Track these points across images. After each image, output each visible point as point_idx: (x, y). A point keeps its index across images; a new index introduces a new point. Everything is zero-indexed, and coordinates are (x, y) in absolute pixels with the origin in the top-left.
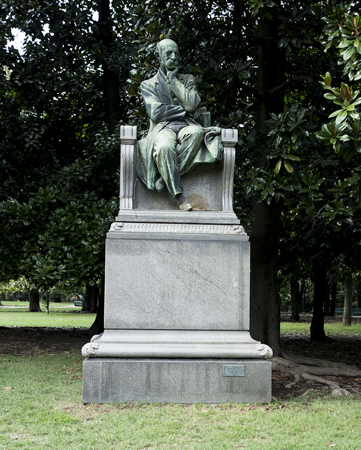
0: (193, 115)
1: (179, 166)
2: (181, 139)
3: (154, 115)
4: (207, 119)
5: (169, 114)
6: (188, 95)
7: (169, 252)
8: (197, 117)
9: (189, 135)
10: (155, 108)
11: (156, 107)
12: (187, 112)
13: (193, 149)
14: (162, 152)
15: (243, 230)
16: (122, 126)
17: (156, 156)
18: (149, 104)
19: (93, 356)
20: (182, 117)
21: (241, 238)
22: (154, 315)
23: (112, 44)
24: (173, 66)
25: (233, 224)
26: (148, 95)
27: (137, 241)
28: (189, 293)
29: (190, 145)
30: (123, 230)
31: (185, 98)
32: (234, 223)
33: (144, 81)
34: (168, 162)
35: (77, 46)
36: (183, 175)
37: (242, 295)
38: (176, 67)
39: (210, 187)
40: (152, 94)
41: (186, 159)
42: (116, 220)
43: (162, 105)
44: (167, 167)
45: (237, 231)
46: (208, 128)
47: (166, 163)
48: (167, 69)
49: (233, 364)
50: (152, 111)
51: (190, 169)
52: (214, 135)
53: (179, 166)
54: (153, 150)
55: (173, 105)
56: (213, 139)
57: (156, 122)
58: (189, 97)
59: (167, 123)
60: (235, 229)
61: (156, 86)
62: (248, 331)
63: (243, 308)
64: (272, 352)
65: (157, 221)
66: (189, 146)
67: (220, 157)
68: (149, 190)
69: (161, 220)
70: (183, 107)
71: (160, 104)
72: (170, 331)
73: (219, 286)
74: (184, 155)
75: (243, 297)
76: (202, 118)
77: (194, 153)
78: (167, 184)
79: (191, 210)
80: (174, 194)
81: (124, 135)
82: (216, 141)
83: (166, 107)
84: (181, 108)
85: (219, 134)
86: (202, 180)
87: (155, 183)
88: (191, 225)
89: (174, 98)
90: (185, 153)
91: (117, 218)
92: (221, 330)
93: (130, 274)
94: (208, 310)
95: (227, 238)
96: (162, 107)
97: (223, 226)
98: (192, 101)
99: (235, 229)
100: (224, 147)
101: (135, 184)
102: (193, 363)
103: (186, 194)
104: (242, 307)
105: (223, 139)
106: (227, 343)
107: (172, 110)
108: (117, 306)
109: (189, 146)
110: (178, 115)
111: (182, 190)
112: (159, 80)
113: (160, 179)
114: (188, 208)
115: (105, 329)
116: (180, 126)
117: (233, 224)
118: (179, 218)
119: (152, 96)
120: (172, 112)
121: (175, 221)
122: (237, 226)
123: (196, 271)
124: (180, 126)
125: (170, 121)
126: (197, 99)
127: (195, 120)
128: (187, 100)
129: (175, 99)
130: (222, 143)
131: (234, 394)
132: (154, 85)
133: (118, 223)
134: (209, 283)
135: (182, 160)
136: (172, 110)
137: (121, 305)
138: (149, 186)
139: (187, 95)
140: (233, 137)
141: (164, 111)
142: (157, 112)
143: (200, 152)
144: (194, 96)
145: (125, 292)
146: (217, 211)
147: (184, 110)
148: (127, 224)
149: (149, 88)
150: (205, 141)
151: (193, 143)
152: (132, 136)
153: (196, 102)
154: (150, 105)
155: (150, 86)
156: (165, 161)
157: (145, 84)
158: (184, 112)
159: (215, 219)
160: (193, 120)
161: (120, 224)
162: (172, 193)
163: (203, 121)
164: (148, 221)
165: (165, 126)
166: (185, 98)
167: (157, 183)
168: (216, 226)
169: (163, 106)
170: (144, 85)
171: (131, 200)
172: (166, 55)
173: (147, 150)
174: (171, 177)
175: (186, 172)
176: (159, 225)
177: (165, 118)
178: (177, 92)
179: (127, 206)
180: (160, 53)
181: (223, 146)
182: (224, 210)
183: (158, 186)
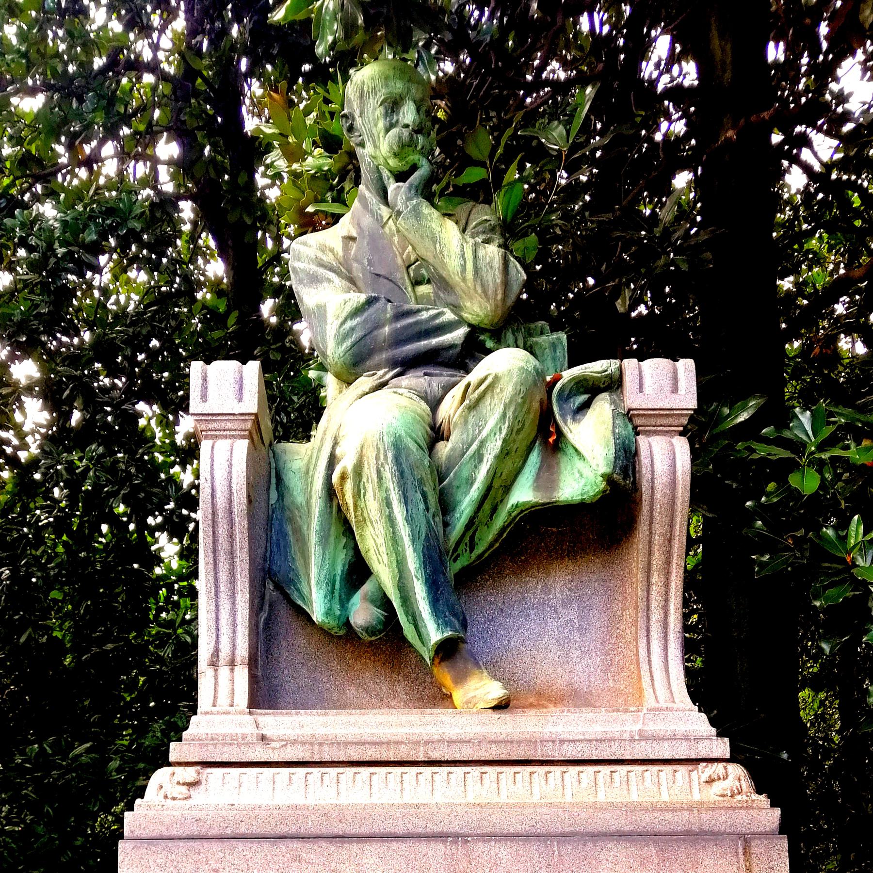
3: (339, 343)
4: (554, 359)
5: (399, 340)
6: (475, 257)
9: (486, 378)
10: (341, 320)
11: (348, 309)
13: (505, 441)
15: (746, 784)
17: (343, 478)
20: (452, 346)
21: (742, 821)
26: (314, 280)
27: (266, 845)
30: (198, 796)
31: (464, 268)
36: (463, 570)
39: (581, 618)
40: (332, 275)
41: (475, 492)
43: (370, 302)
44: (391, 520)
45: (719, 787)
47: (388, 504)
48: (386, 173)
51: (495, 540)
56: (586, 406)
57: (347, 379)
58: (481, 263)
59: (391, 374)
60: (710, 781)
61: (346, 249)
65: (355, 758)
66: (484, 433)
68: (320, 629)
70: (456, 308)
71: (362, 298)
77: (509, 465)
78: (396, 603)
79: (502, 706)
81: (204, 397)
83: (385, 311)
87: (344, 602)
95: (680, 821)
96: (371, 310)
97: (654, 769)
98: (490, 279)
101: (264, 616)
103: (475, 642)
107: (411, 320)
109: (484, 433)
110: (434, 341)
111: (464, 625)
112: (359, 226)
113: (368, 587)
118: (451, 742)
119: (329, 281)
120: (410, 331)
121: (435, 755)
122: (719, 768)
125: (406, 365)
126: (512, 272)
128: (470, 274)
130: (629, 416)
136: (411, 320)
138: (318, 613)
139: (469, 255)
140: (675, 390)
141: (378, 326)
142: (352, 329)
143: (534, 458)
147: (461, 322)
149: (320, 255)
151: (504, 415)
152: (240, 400)
156: (381, 495)
161: (190, 773)
164: (316, 758)
166: (464, 268)
168: (622, 769)
172: (379, 111)
173: (307, 472)
174: (413, 562)
176: (365, 771)
177: (384, 356)
178: (428, 243)
180: (357, 114)
181: (635, 428)
182: (649, 701)
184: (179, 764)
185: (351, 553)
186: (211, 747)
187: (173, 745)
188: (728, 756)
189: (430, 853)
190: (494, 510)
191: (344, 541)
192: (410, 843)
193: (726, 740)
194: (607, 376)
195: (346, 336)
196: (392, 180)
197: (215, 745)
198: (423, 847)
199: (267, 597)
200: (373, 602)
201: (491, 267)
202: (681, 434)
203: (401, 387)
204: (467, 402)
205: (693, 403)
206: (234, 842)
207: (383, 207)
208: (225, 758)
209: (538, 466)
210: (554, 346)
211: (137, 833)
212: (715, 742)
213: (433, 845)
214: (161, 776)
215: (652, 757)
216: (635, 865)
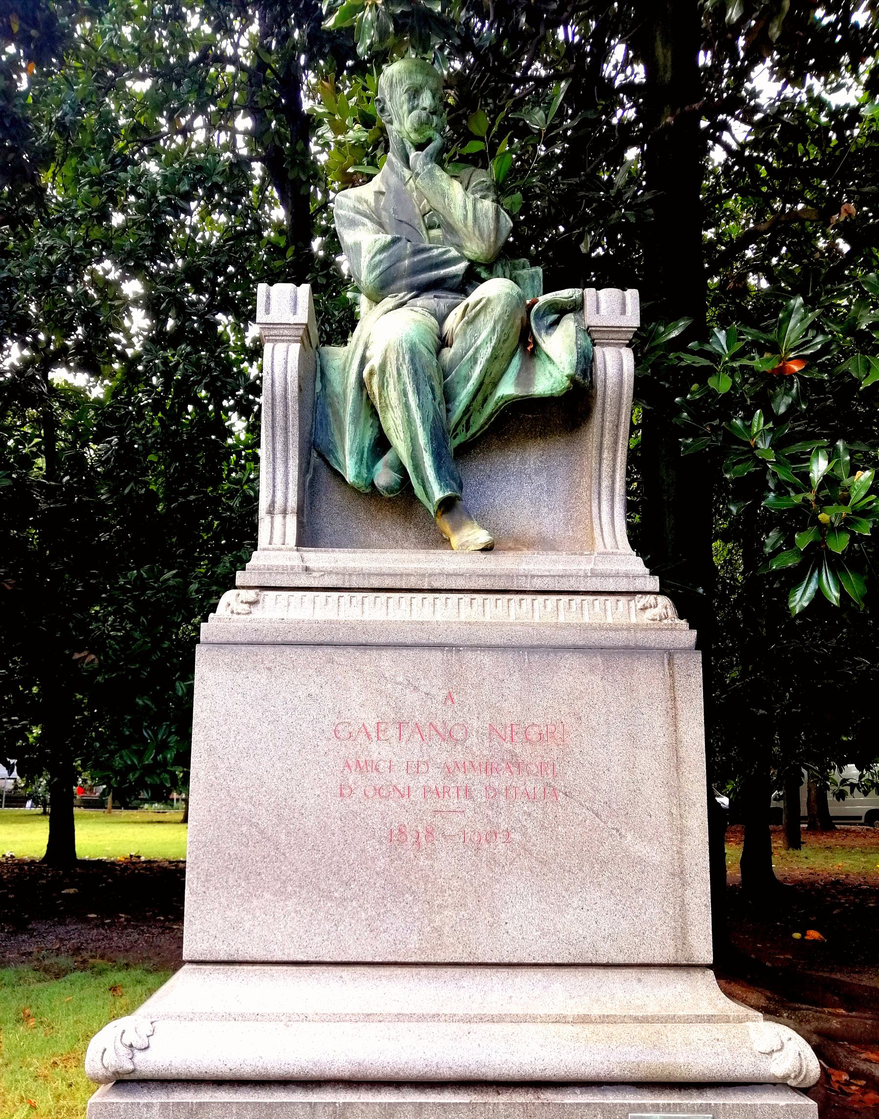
3: (371, 272)
4: (532, 287)
5: (416, 270)
7: (416, 689)
9: (480, 301)
10: (372, 254)
11: (378, 246)
12: (473, 264)
13: (494, 348)
14: (392, 357)
15: (671, 611)
16: (262, 288)
19: (126, 1077)
20: (455, 276)
21: (667, 639)
22: (366, 910)
25: (635, 593)
26: (353, 224)
29: (484, 334)
30: (257, 613)
31: (466, 217)
32: (639, 589)
34: (410, 389)
37: (682, 832)
39: (549, 483)
40: (366, 221)
41: (470, 387)
42: (238, 583)
43: (394, 241)
44: (407, 406)
45: (650, 613)
47: (405, 395)
48: (408, 144)
52: (561, 311)
54: (363, 361)
55: (427, 244)
56: (556, 323)
59: (409, 296)
60: (644, 609)
62: (709, 967)
66: (479, 342)
67: (584, 373)
68: (353, 489)
69: (388, 583)
70: (459, 247)
71: (389, 238)
72: (423, 971)
75: (682, 841)
77: (497, 367)
78: (410, 470)
79: (487, 549)
81: (267, 311)
82: (568, 324)
84: (454, 253)
85: (577, 307)
86: (523, 462)
87: (370, 467)
88: (492, 597)
90: (467, 367)
93: (278, 765)
98: (485, 225)
99: (644, 609)
101: (309, 477)
102: (513, 1105)
104: (680, 875)
106: (637, 1020)
107: (425, 256)
108: (231, 882)
109: (479, 342)
110: (442, 272)
111: (461, 487)
112: (387, 183)
113: (388, 457)
114: (479, 541)
115: (184, 962)
116: (449, 301)
117: (635, 593)
118: (449, 575)
119: (364, 225)
120: (425, 264)
121: (437, 585)
122: (651, 599)
124: (449, 301)
126: (503, 221)
130: (588, 331)
133: (242, 592)
135: (458, 390)
136: (425, 256)
137: (247, 878)
138: (350, 472)
139: (470, 207)
140: (623, 312)
141: (400, 259)
142: (381, 261)
143: (516, 362)
145: (262, 832)
148: (272, 594)
149: (357, 205)
150: (533, 325)
151: (494, 329)
152: (295, 313)
153: (497, 229)
155: (360, 200)
158: (462, 266)
159: (571, 576)
161: (251, 595)
164: (347, 585)
166: (466, 217)
167: (380, 466)
168: (577, 598)
169: (400, 244)
171: (292, 522)
173: (344, 369)
174: (423, 439)
175: (473, 431)
176: (383, 596)
178: (439, 198)
179: (277, 539)
182: (600, 548)
183: (383, 476)
185: (376, 430)
188: (658, 590)
191: (371, 421)
192: (417, 650)
193: (657, 577)
194: (572, 301)
195: (375, 267)
196: (413, 149)
198: (426, 654)
199: (312, 463)
200: (392, 468)
201: (486, 217)
202: (628, 346)
205: (636, 322)
210: (532, 277)
211: (210, 639)
212: (648, 579)
216: (586, 671)
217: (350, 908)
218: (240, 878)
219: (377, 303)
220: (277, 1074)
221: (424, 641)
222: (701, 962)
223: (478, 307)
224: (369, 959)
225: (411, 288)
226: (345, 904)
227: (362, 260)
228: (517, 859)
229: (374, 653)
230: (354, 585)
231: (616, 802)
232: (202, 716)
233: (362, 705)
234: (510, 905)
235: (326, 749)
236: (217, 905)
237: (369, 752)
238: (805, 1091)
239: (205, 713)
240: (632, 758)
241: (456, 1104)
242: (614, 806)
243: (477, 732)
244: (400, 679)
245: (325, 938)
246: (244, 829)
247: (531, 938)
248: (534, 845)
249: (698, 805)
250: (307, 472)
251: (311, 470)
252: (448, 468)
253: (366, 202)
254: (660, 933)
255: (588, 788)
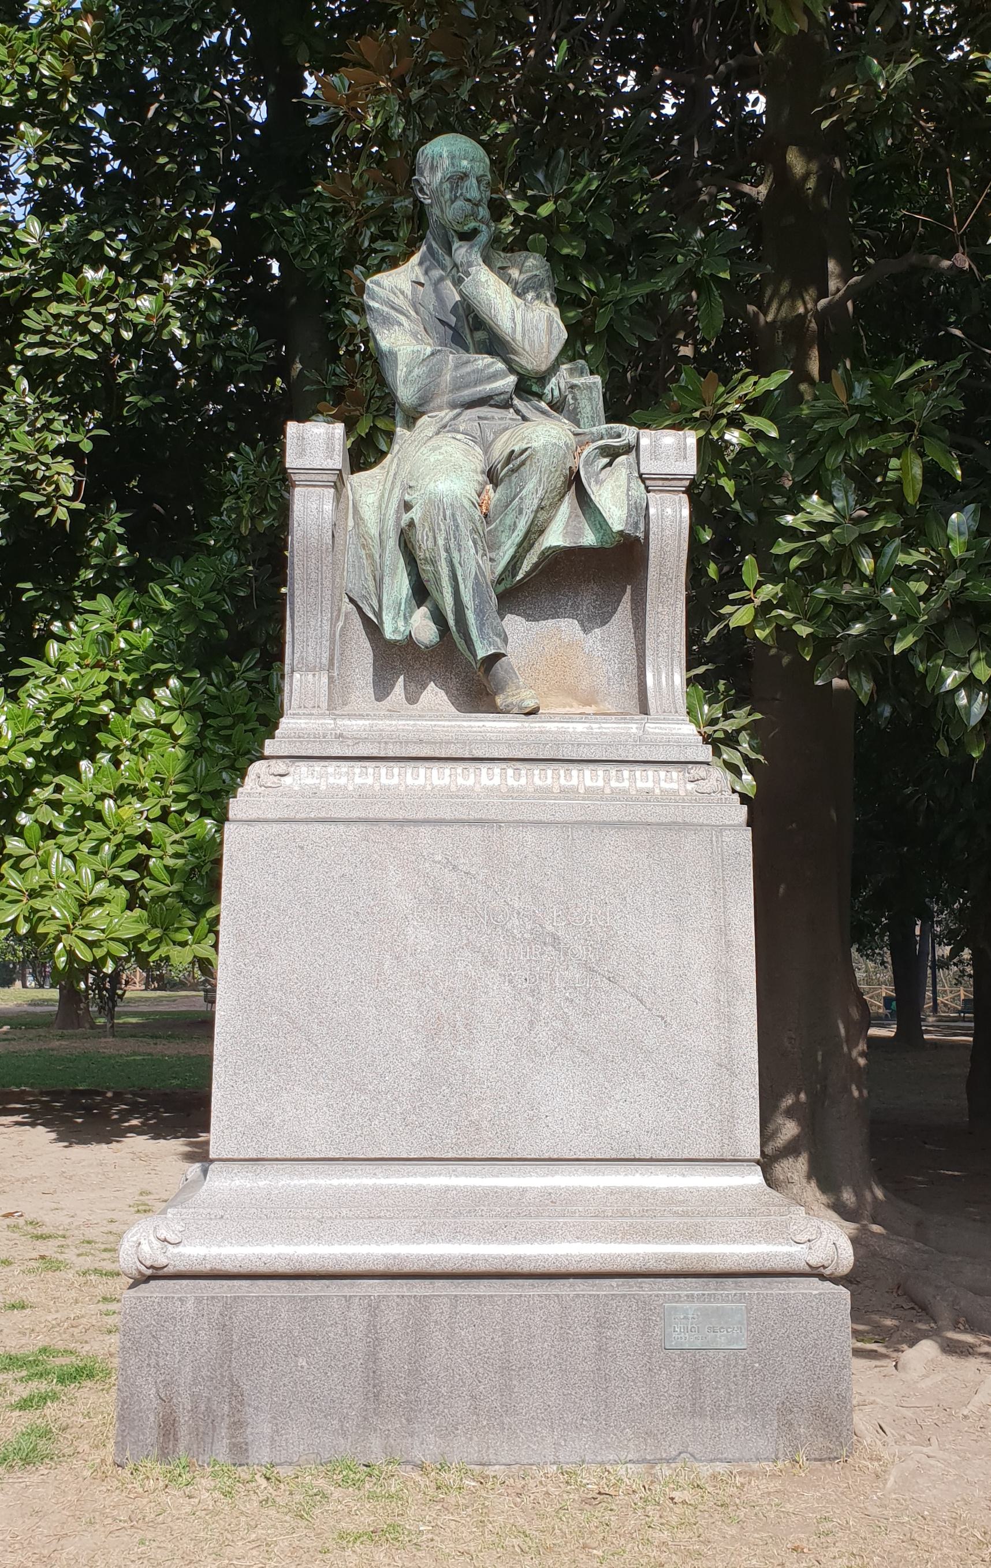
0: (544, 386)
1: (491, 560)
2: (499, 466)
4: (590, 399)
5: (458, 386)
8: (556, 393)
18: (590, 631)
23: (709, 623)
24: (473, 224)
28: (531, 1023)
33: (376, 277)
35: (159, 399)
38: (484, 228)
40: (402, 319)
46: (594, 429)
49: (701, 1298)
50: (401, 372)
52: (612, 454)
53: (491, 560)
56: (610, 464)
63: (733, 1074)
64: (851, 1251)
68: (392, 644)
73: (640, 993)
74: (508, 521)
75: (730, 1029)
76: (575, 398)
78: (451, 622)
80: (475, 655)
81: (302, 453)
89: (477, 329)
91: (270, 747)
92: (651, 1160)
94: (601, 1080)
100: (648, 491)
101: (340, 624)
105: (648, 467)
119: (400, 324)
123: (555, 938)
126: (555, 332)
127: (549, 404)
129: (480, 335)
131: (708, 1422)
132: (407, 287)
134: (605, 984)
137: (277, 1071)
144: (543, 325)
146: (622, 715)
149: (392, 297)
153: (550, 342)
154: (393, 354)
157: (378, 284)
160: (543, 405)
161: (280, 766)
162: (467, 654)
163: (575, 408)
164: (382, 755)
165: (445, 427)
169: (438, 357)
170: (376, 288)
181: (646, 488)
184: (273, 757)
186: (298, 744)
187: (267, 742)
189: (472, 835)
190: (531, 546)
192: (456, 826)
194: (624, 445)
196: (456, 239)
197: (301, 742)
198: (466, 830)
199: (343, 610)
201: (537, 329)
202: (684, 492)
203: (459, 432)
204: (511, 466)
206: (316, 824)
207: (447, 257)
208: (309, 753)
209: (567, 516)
211: (239, 817)
212: (700, 748)
213: (474, 828)
214: (257, 768)
215: (650, 759)
217: (384, 1102)
218: (269, 1070)
219: (429, 594)
220: (312, 1269)
221: (463, 817)
222: (748, 1157)
223: (524, 456)
224: (405, 1156)
225: (453, 406)
226: (380, 1097)
227: (399, 373)
228: (558, 1049)
229: (411, 830)
230: (391, 754)
231: (661, 988)
232: (231, 898)
233: (399, 886)
234: (550, 1097)
235: (361, 933)
236: (245, 1100)
237: (405, 935)
238: (835, 1280)
239: (233, 896)
240: (678, 941)
241: (492, 1296)
242: (659, 992)
243: (519, 913)
244: (438, 858)
245: (359, 1133)
246: (274, 1018)
247: (572, 1131)
248: (576, 1033)
249: (747, 992)
250: (338, 620)
251: (342, 618)
252: (492, 623)
253: (402, 293)
254: (705, 1126)
255: (632, 973)
